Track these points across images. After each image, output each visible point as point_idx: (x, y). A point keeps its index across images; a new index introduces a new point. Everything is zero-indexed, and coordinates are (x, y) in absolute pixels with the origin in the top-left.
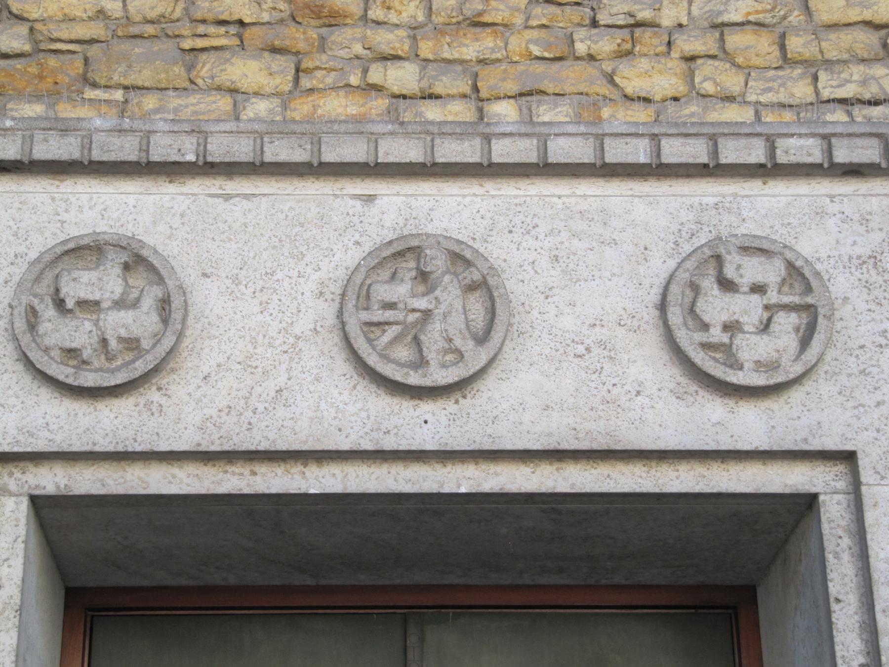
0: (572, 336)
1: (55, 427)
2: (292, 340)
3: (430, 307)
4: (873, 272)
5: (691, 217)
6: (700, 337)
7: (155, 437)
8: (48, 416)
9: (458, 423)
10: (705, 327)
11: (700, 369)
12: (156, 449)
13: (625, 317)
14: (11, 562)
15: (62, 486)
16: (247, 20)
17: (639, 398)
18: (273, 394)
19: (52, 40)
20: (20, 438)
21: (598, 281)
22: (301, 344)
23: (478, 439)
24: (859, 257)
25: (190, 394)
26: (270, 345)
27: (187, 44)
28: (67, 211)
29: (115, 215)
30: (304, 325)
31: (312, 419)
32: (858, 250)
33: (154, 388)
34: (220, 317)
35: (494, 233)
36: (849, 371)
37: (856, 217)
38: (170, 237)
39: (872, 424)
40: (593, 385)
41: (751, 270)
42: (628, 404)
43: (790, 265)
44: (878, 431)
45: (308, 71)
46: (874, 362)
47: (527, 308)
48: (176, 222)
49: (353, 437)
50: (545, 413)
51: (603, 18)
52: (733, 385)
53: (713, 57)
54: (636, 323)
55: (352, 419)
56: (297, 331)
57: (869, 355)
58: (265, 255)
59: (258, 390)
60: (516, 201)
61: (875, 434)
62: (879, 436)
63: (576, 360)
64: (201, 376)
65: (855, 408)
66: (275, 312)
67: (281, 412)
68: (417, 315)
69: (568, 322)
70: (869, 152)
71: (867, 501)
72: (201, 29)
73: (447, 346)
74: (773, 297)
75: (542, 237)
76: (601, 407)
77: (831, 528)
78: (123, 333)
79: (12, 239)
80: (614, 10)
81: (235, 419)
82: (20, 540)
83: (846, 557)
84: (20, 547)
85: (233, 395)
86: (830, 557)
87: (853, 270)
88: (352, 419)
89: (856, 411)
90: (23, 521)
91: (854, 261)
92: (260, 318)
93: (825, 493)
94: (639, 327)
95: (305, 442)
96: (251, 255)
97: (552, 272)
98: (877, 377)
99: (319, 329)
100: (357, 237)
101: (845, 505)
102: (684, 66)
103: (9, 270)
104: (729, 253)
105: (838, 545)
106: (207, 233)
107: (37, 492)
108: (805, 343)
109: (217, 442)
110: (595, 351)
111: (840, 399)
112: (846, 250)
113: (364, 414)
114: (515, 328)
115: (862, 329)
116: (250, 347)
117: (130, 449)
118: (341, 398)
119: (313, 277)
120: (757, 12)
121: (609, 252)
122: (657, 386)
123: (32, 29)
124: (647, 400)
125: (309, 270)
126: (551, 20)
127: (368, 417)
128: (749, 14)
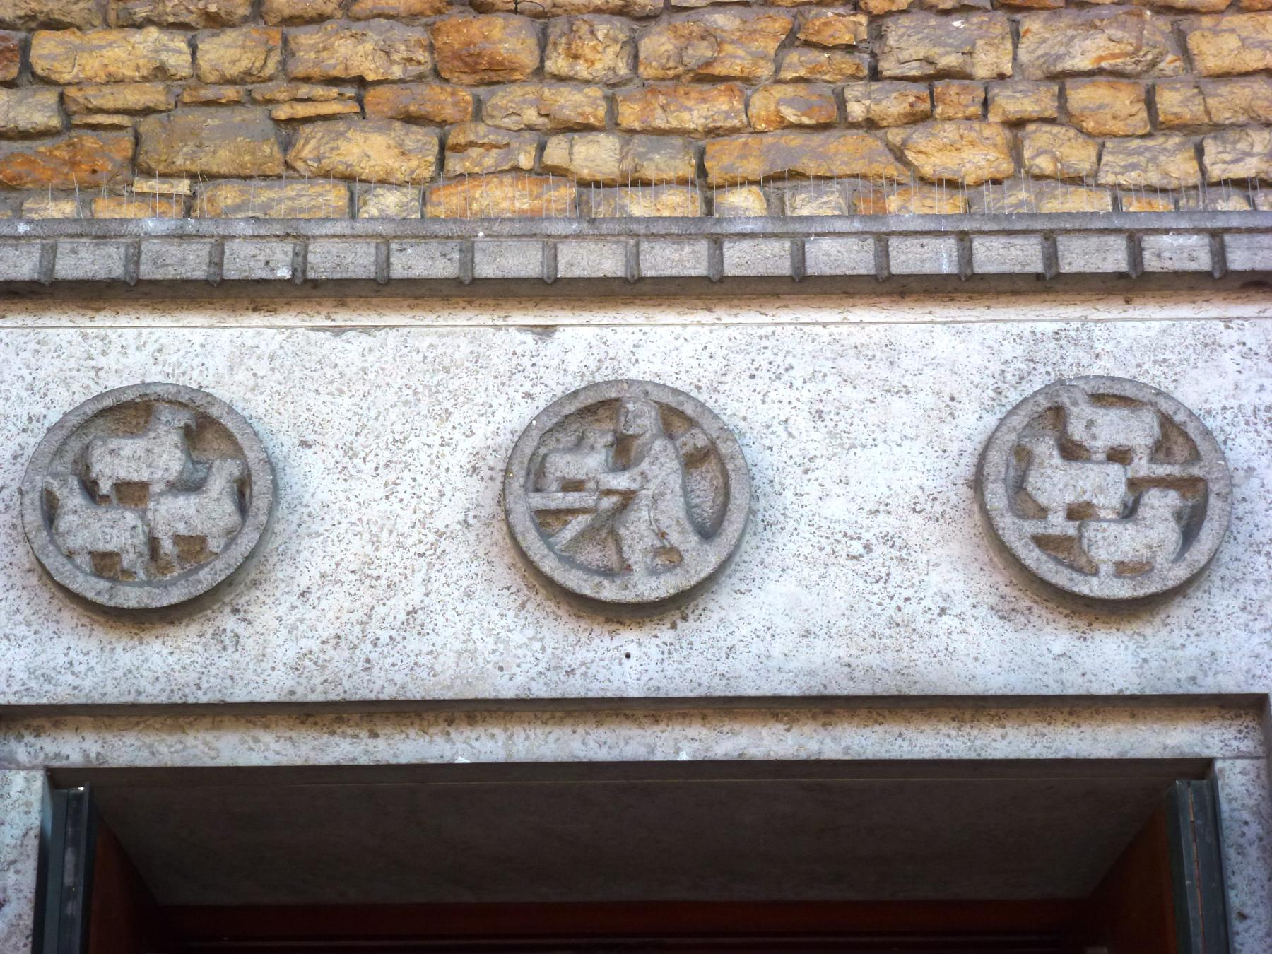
0: (844, 527)
2: (431, 538)
3: (634, 486)
5: (1019, 351)
6: (1031, 527)
7: (228, 682)
8: (72, 653)
9: (675, 656)
10: (1042, 512)
12: (229, 700)
13: (922, 499)
15: (93, 755)
16: (371, 77)
17: (945, 618)
18: (402, 616)
22: (444, 544)
23: (705, 681)
25: (280, 619)
26: (399, 545)
27: (283, 113)
28: (104, 353)
29: (174, 359)
31: (459, 653)
33: (227, 610)
34: (325, 506)
35: (729, 378)
36: (1256, 576)
38: (253, 389)
40: (875, 599)
41: (1111, 428)
42: (927, 627)
43: (1166, 421)
47: (777, 488)
48: (263, 368)
49: (520, 679)
50: (805, 641)
51: (889, 67)
54: (938, 508)
55: (520, 652)
56: (439, 523)
58: (393, 415)
59: (381, 611)
60: (762, 332)
63: (850, 563)
64: (297, 591)
66: (407, 497)
67: (414, 644)
68: (615, 499)
69: (837, 508)
72: (304, 91)
73: (658, 544)
74: (1142, 467)
75: (798, 383)
76: (888, 632)
77: (1233, 810)
78: (182, 529)
79: (24, 394)
80: (905, 55)
81: (346, 654)
87: (1260, 427)
88: (520, 652)
90: (36, 806)
92: (384, 505)
93: (1224, 758)
96: (373, 413)
97: (814, 435)
99: (471, 520)
100: (527, 386)
101: (1252, 775)
102: (1007, 133)
104: (1075, 404)
105: (1243, 834)
106: (308, 384)
107: (56, 764)
109: (320, 688)
110: (879, 549)
111: (1244, 617)
112: (1249, 399)
116: (369, 549)
118: (503, 622)
120: (1114, 56)
122: (971, 600)
123: (62, 98)
124: (956, 621)
125: (457, 435)
127: (543, 649)
128: (1101, 58)
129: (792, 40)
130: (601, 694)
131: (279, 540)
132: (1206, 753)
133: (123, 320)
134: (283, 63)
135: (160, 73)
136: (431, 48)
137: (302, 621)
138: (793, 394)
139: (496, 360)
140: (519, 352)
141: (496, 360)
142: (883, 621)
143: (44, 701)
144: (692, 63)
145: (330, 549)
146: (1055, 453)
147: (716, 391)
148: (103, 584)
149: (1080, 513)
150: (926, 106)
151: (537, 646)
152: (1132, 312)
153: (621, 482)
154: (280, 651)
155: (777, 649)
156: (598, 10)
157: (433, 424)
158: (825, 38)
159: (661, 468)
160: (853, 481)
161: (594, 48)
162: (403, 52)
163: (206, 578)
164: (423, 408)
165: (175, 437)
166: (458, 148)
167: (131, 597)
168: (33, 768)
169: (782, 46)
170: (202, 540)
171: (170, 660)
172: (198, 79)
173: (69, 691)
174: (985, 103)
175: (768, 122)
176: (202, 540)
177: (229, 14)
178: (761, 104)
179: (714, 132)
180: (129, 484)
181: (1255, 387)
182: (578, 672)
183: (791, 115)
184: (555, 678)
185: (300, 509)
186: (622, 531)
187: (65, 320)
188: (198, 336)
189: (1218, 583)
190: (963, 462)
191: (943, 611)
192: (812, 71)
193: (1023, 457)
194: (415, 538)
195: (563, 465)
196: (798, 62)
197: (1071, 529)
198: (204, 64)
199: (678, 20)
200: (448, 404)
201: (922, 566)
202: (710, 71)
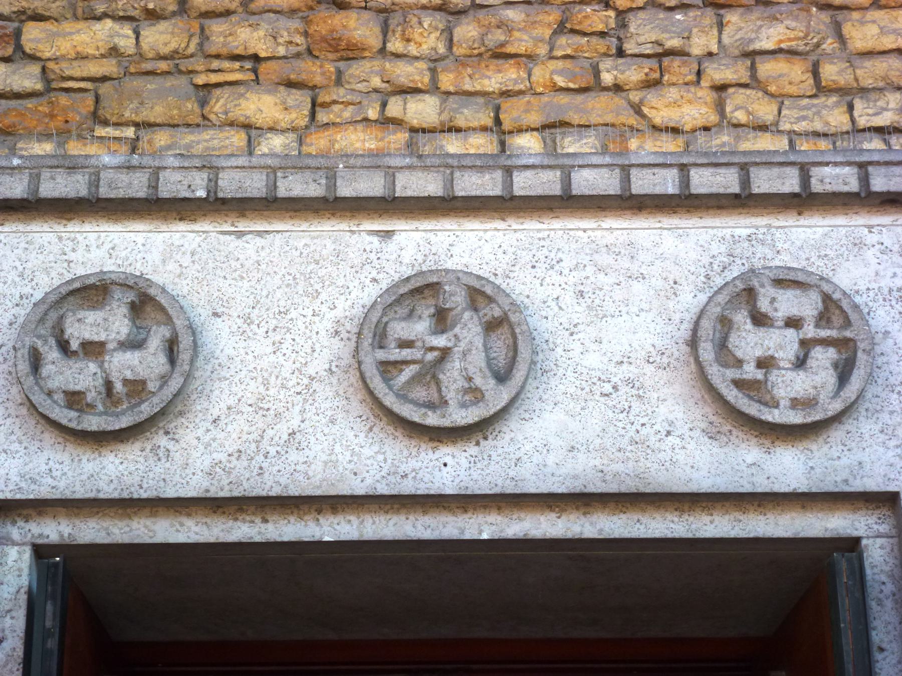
0: (599, 374)
3: (449, 345)
5: (723, 249)
6: (731, 373)
7: (162, 484)
8: (51, 462)
9: (479, 465)
10: (739, 363)
12: (162, 496)
13: (654, 353)
14: (14, 614)
15: (66, 535)
16: (263, 54)
17: (670, 438)
18: (285, 437)
22: (315, 385)
23: (500, 482)
25: (198, 439)
26: (283, 386)
27: (200, 80)
28: (74, 250)
29: (123, 254)
31: (326, 463)
33: (161, 432)
35: (517, 268)
38: (179, 276)
40: (620, 425)
41: (788, 303)
43: (827, 298)
47: (551, 346)
48: (186, 261)
49: (369, 481)
50: (571, 454)
51: (630, 47)
54: (665, 360)
55: (369, 462)
56: (311, 371)
58: (279, 294)
59: (270, 433)
60: (540, 235)
63: (602, 399)
64: (211, 419)
66: (288, 352)
67: (293, 456)
68: (436, 353)
69: (593, 360)
72: (215, 64)
73: (466, 385)
74: (810, 331)
75: (566, 272)
76: (629, 448)
77: (874, 574)
78: (129, 375)
79: (17, 279)
80: (642, 39)
81: (246, 463)
87: (893, 303)
88: (369, 462)
90: (26, 571)
91: (894, 293)
92: (272, 358)
93: (868, 537)
96: (264, 293)
97: (577, 308)
99: (334, 369)
100: (374, 274)
101: (888, 549)
102: (714, 95)
104: (763, 286)
105: (882, 591)
106: (218, 272)
107: (40, 541)
109: (227, 488)
110: (624, 389)
111: (882, 437)
112: (886, 283)
113: (381, 457)
116: (262, 389)
118: (356, 441)
120: (790, 40)
121: (638, 287)
123: (44, 69)
124: (678, 440)
125: (324, 308)
126: (576, 50)
127: (385, 460)
128: (781, 41)
129: (561, 28)
130: (426, 492)
131: (198, 383)
132: (855, 534)
133: (87, 227)
134: (201, 45)
135: (114, 51)
136: (306, 34)
137: (214, 440)
138: (562, 279)
139: (352, 255)
140: (368, 250)
141: (352, 255)
142: (626, 440)
143: (32, 497)
144: (491, 45)
145: (234, 389)
146: (748, 321)
147: (508, 277)
148: (73, 414)
149: (765, 363)
150: (656, 75)
151: (381, 457)
152: (803, 221)
153: (441, 341)
154: (199, 461)
155: (551, 460)
156: (424, 7)
157: (307, 301)
158: (585, 27)
159: (469, 331)
160: (605, 341)
161: (421, 34)
162: (286, 37)
163: (146, 409)
164: (300, 289)
165: (124, 310)
166: (325, 105)
167: (93, 423)
168: (24, 544)
169: (555, 33)
170: (143, 382)
171: (121, 468)
172: (141, 56)
173: (49, 489)
174: (699, 73)
175: (545, 86)
176: (143, 382)
177: (163, 10)
178: (540, 74)
179: (506, 94)
180: (91, 343)
181: (890, 274)
182: (410, 477)
183: (561, 82)
184: (394, 481)
185: (213, 361)
186: (441, 376)
187: (46, 227)
188: (140, 238)
189: (864, 413)
190: (683, 327)
191: (669, 433)
193: (725, 323)
194: (294, 381)
195: (400, 329)
196: (566, 44)
197: (759, 375)
198: (145, 45)
199: (481, 14)
200: (318, 287)
201: (654, 401)
202: (504, 50)
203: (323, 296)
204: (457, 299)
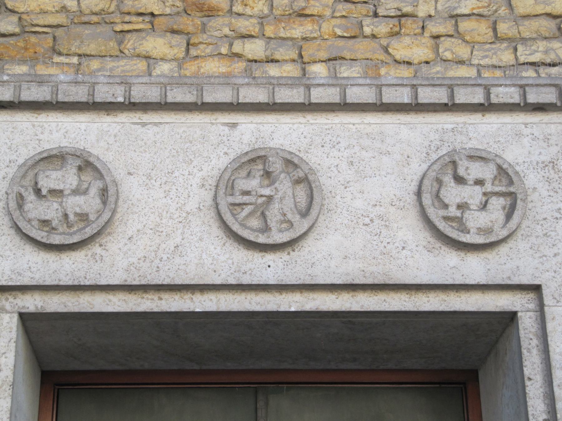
0: (362, 212)
1: (35, 269)
3: (272, 194)
4: (552, 172)
5: (437, 137)
7: (98, 276)
8: (30, 263)
9: (289, 267)
10: (446, 206)
11: (443, 233)
12: (98, 284)
13: (395, 200)
14: (7, 355)
15: (39, 307)
16: (156, 13)
17: (404, 251)
19: (33, 25)
20: (13, 276)
21: (378, 177)
22: (190, 217)
23: (302, 277)
24: (543, 162)
25: (120, 249)
26: (171, 218)
27: (118, 28)
28: (42, 133)
29: (73, 136)
30: (192, 205)
31: (197, 265)
32: (543, 158)
34: (139, 200)
36: (537, 234)
37: (541, 137)
38: (107, 150)
39: (551, 268)
40: (375, 243)
41: (475, 171)
42: (397, 255)
43: (500, 167)
44: (555, 272)
45: (195, 45)
46: (552, 229)
47: (333, 195)
48: (111, 140)
49: (223, 276)
50: (345, 261)
51: (381, 11)
52: (463, 243)
53: (451, 36)
54: (402, 204)
55: (223, 264)
56: (188, 209)
57: (549, 224)
58: (168, 161)
59: (163, 246)
60: (327, 127)
61: (553, 274)
62: (556, 275)
63: (364, 227)
64: (127, 237)
65: (540, 257)
66: (174, 197)
67: (178, 260)
68: (264, 199)
69: (359, 203)
70: (550, 96)
71: (548, 316)
72: (127, 18)
73: (283, 219)
74: (489, 187)
75: (342, 149)
77: (525, 333)
78: (78, 210)
79: (7, 151)
81: (149, 265)
82: (13, 341)
83: (535, 351)
84: (13, 345)
85: (147, 250)
86: (524, 351)
87: (539, 170)
88: (223, 264)
89: (541, 260)
90: (15, 329)
91: (540, 165)
92: (164, 200)
93: (522, 311)
94: (404, 206)
95: (193, 279)
96: (159, 161)
98: (554, 238)
99: (201, 207)
100: (226, 150)
101: (534, 319)
102: (432, 41)
103: (5, 170)
104: (461, 160)
105: (530, 344)
106: (131, 147)
107: (23, 311)
108: (509, 216)
109: (138, 279)
110: (376, 221)
111: (531, 252)
112: (535, 158)
113: (230, 261)
114: (326, 207)
115: (545, 207)
116: (158, 219)
117: (82, 284)
118: (216, 251)
119: (198, 175)
120: (479, 8)
121: (385, 159)
122: (415, 244)
123: (20, 19)
124: (409, 253)
125: (195, 170)
127: (233, 263)
128: (473, 9)
164: (181, 158)
176: (87, 215)
192: (348, 13)
194: (178, 214)
203: (195, 163)
204: (276, 166)
